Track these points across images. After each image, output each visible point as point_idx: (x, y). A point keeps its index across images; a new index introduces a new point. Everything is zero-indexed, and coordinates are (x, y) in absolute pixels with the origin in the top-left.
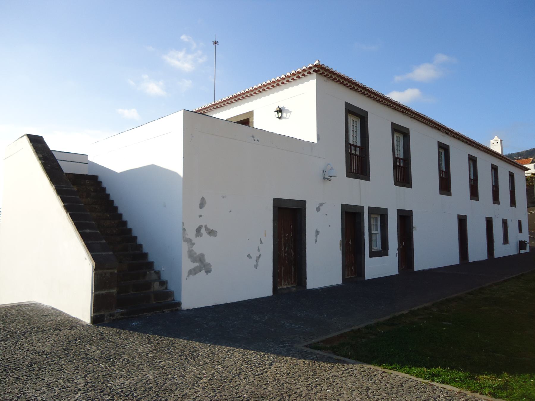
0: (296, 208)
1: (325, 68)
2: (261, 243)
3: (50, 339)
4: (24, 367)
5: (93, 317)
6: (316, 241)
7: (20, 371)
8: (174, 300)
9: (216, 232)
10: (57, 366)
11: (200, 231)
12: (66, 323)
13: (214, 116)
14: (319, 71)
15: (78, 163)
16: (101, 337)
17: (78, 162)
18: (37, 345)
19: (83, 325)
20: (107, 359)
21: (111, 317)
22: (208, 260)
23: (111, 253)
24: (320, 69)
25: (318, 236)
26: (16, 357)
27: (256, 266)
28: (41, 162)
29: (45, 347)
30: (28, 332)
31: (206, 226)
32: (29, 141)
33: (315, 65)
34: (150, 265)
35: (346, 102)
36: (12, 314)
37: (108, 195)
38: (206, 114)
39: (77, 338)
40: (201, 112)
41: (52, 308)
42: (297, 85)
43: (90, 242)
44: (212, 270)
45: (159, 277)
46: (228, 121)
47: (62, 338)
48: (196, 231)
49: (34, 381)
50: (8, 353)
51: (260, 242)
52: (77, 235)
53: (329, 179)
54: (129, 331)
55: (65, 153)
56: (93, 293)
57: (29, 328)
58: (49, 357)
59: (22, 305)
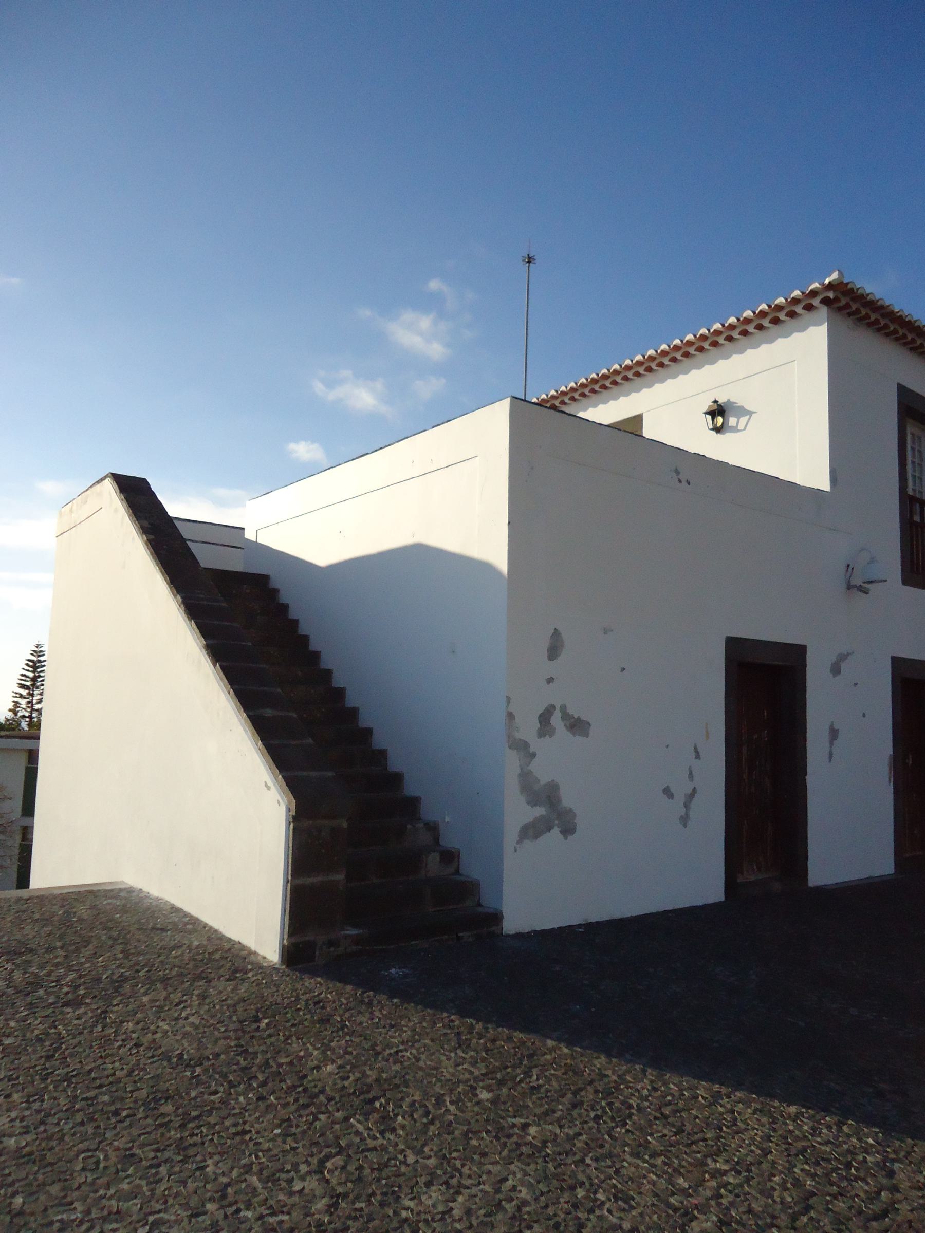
0: (780, 663)
2: (698, 756)
3: (188, 1011)
5: (288, 947)
6: (831, 756)
7: (130, 1126)
8: (480, 905)
9: (589, 724)
10: (229, 1115)
11: (549, 720)
13: (581, 414)
14: (836, 299)
16: (320, 1013)
19: (261, 967)
21: (332, 949)
22: (568, 799)
24: (840, 296)
27: (685, 820)
28: (147, 537)
31: (563, 709)
32: (118, 491)
33: (829, 282)
36: (80, 920)
37: (295, 622)
43: (277, 742)
44: (579, 827)
45: (437, 840)
48: (540, 722)
50: (88, 1051)
51: (694, 755)
56: (288, 882)
59: (99, 891)
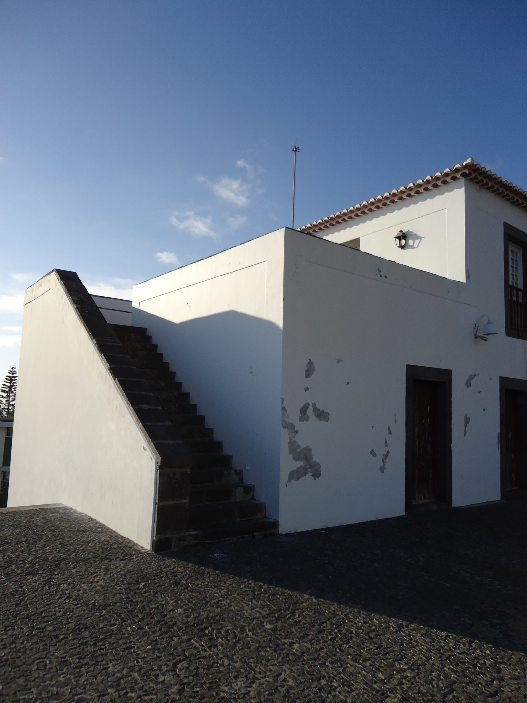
0: (435, 380)
1: (480, 170)
2: (390, 433)
3: (98, 578)
4: (69, 634)
5: (156, 541)
6: (465, 433)
12: (115, 546)
13: (325, 238)
14: (470, 174)
15: (116, 311)
16: (174, 579)
17: (116, 310)
18: (81, 587)
20: (198, 627)
21: (181, 542)
22: (316, 458)
23: (181, 442)
25: (467, 425)
26: (53, 610)
27: (382, 469)
29: (95, 594)
30: (63, 559)
31: (314, 405)
33: (466, 164)
34: (227, 460)
35: (504, 223)
36: (36, 526)
37: (161, 355)
38: (315, 234)
39: (138, 578)
40: (309, 232)
41: (90, 519)
42: (451, 191)
45: (241, 479)
46: (345, 246)
47: (115, 576)
48: (301, 413)
49: (92, 669)
51: (388, 431)
52: (131, 412)
53: (485, 337)
54: (215, 570)
55: (101, 298)
56: (156, 504)
57: (65, 553)
58: (105, 615)
59: (47, 509)
